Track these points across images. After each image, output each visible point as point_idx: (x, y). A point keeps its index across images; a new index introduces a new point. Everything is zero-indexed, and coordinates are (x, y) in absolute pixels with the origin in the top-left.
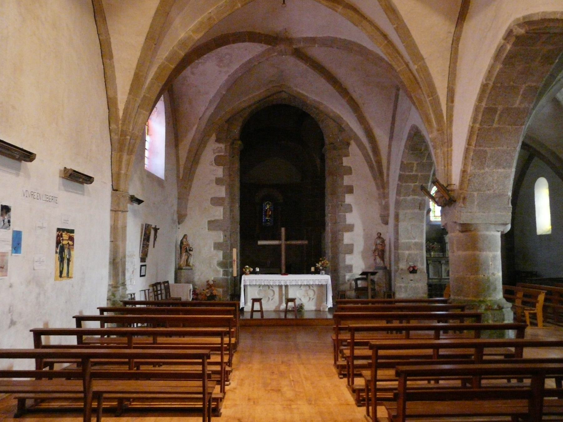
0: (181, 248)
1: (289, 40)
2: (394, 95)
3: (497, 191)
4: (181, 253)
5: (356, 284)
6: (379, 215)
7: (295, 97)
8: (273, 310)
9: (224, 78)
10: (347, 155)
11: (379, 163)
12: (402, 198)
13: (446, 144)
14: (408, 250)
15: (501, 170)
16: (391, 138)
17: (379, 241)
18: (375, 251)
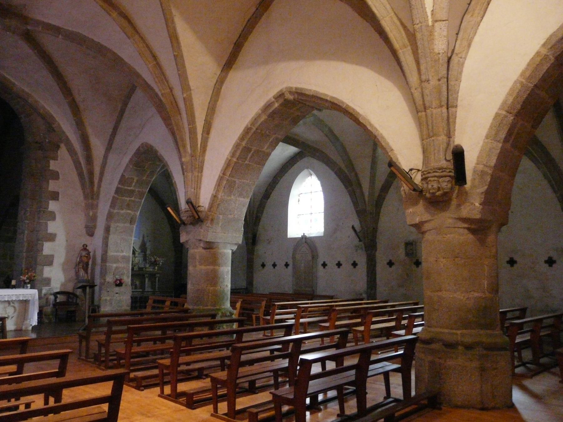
1: (25, 19)
3: (236, 216)
5: (56, 298)
10: (55, 158)
12: (116, 211)
13: (197, 169)
14: (115, 263)
15: (242, 199)
16: (109, 148)
18: (79, 263)
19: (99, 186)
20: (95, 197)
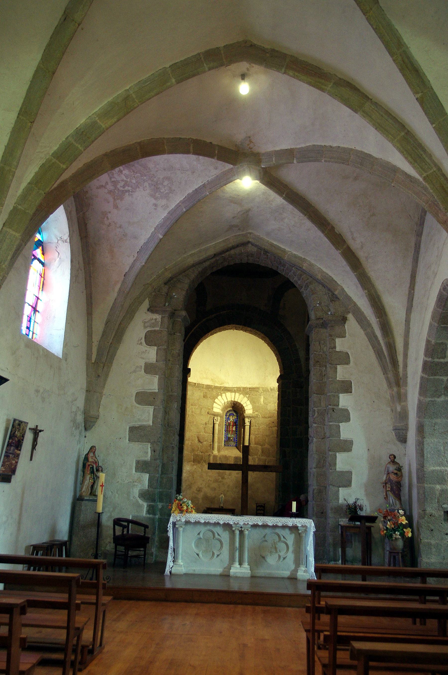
0: (84, 465)
2: (413, 244)
4: (84, 476)
6: (391, 428)
7: (266, 252)
8: (218, 573)
9: (162, 215)
10: (343, 336)
11: (391, 347)
14: (439, 483)
17: (392, 468)
18: (386, 483)
19: (405, 366)
20: (401, 382)
